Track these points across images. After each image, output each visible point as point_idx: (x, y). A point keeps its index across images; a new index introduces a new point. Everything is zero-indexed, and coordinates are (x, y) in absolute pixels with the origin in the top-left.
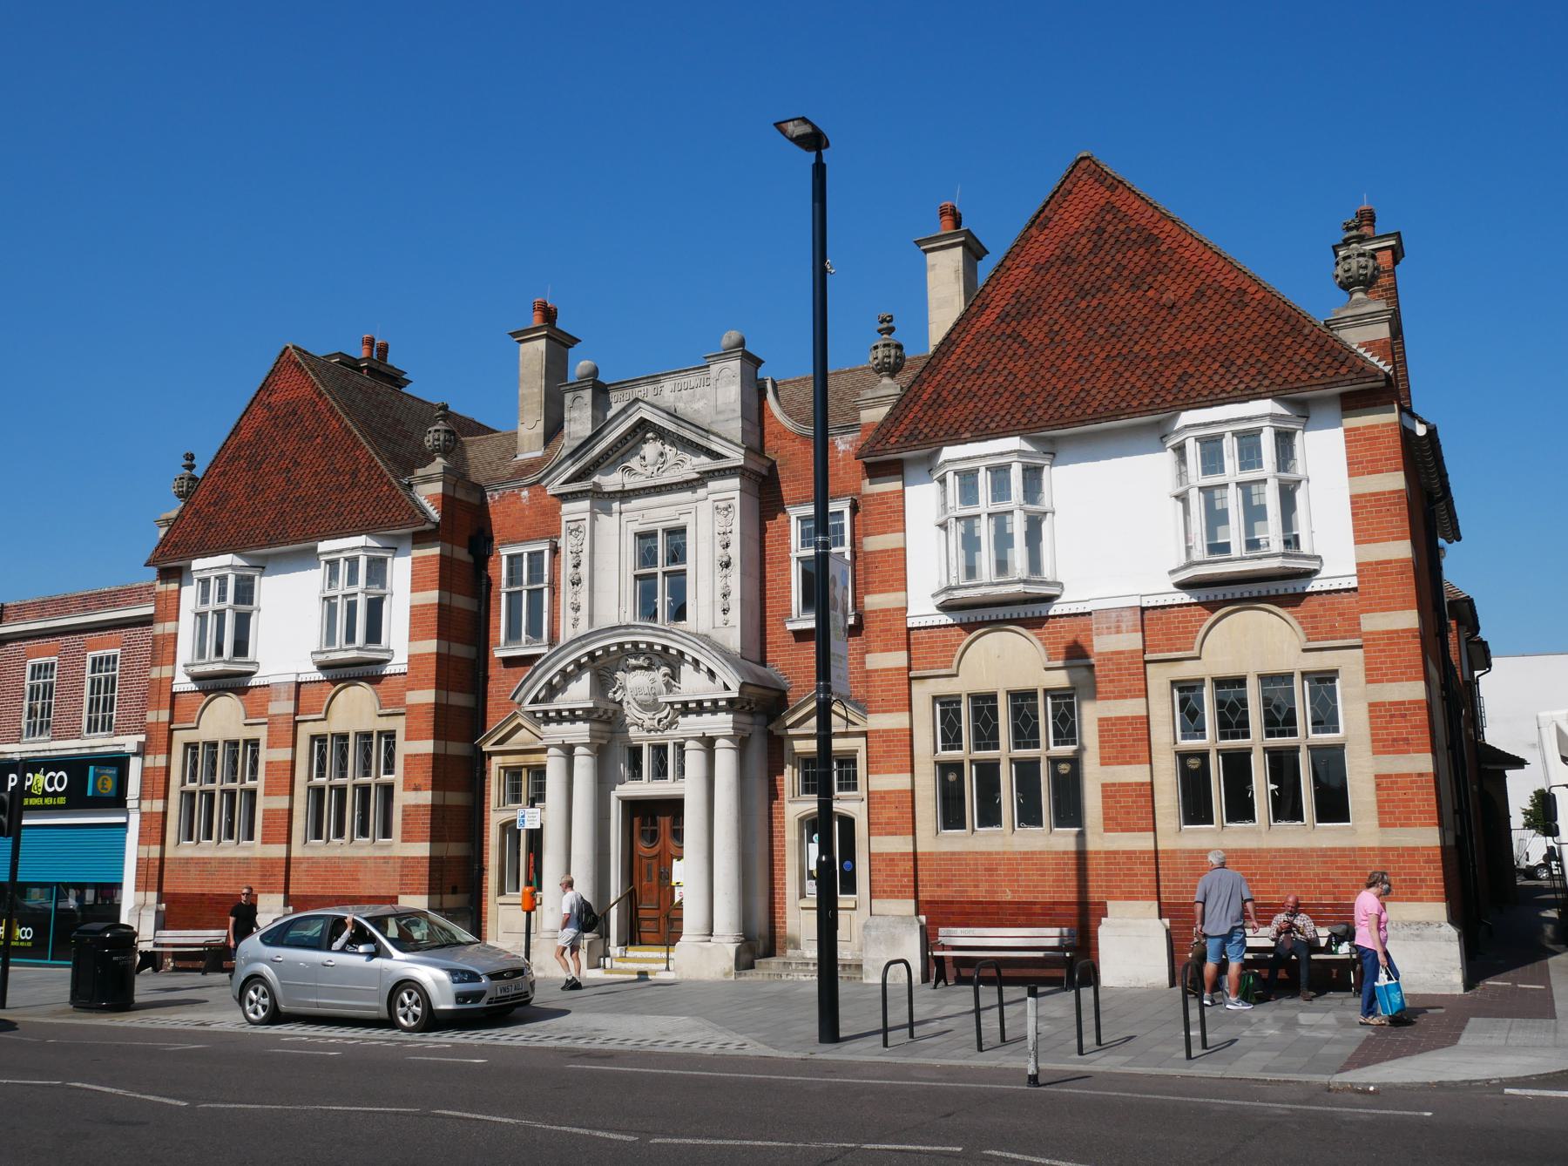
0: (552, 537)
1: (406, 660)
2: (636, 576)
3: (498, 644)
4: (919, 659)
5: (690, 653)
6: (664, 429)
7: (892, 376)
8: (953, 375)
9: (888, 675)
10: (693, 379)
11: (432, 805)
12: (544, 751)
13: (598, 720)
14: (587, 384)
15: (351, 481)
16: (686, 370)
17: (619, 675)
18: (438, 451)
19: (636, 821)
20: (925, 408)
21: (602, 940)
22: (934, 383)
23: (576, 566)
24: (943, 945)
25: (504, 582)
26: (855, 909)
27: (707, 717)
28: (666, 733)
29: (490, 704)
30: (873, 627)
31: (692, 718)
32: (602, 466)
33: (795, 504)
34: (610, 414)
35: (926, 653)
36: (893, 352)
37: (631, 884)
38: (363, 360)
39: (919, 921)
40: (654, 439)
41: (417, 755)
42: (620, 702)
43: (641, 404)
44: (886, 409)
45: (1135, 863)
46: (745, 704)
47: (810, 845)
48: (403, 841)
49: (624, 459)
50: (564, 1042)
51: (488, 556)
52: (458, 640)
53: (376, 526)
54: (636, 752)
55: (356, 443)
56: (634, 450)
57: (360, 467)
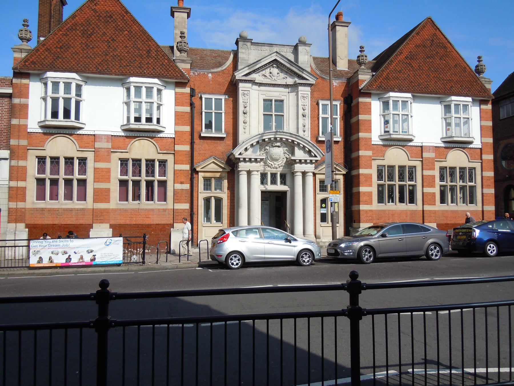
28: (272, 169)
45: (431, 213)
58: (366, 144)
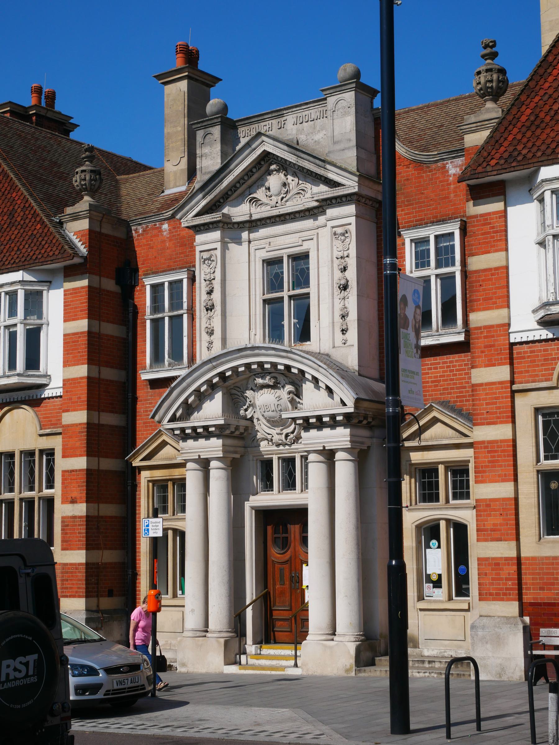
0: (190, 267)
1: (61, 385)
2: (265, 301)
3: (145, 368)
4: (521, 372)
5: (310, 372)
6: (286, 160)
7: (495, 100)
8: (550, 96)
9: (492, 389)
10: (313, 112)
11: (87, 517)
12: (182, 465)
13: (231, 436)
14: (216, 121)
15: (9, 221)
16: (307, 104)
17: (249, 393)
18: (86, 190)
19: (270, 529)
20: (524, 129)
21: (237, 639)
22: (532, 105)
23: (210, 293)
24: (544, 645)
25: (148, 310)
26: (468, 610)
27: (327, 431)
28: (293, 446)
29: (140, 423)
30: (478, 344)
31: (313, 432)
32: (229, 199)
33: (409, 228)
34: (238, 148)
35: (529, 367)
36: (495, 76)
37: (266, 586)
38: (31, 108)
39: (523, 622)
40: (278, 171)
41: (73, 471)
42: (251, 419)
43: (264, 138)
44: (486, 134)
46: (361, 419)
47: (428, 550)
48: (63, 549)
49: (251, 191)
50: (165, 730)
51: (134, 286)
52: (108, 365)
53: (31, 262)
54: (267, 465)
55: (13, 187)
56: (260, 182)
57: (16, 207)
58: (491, 346)
